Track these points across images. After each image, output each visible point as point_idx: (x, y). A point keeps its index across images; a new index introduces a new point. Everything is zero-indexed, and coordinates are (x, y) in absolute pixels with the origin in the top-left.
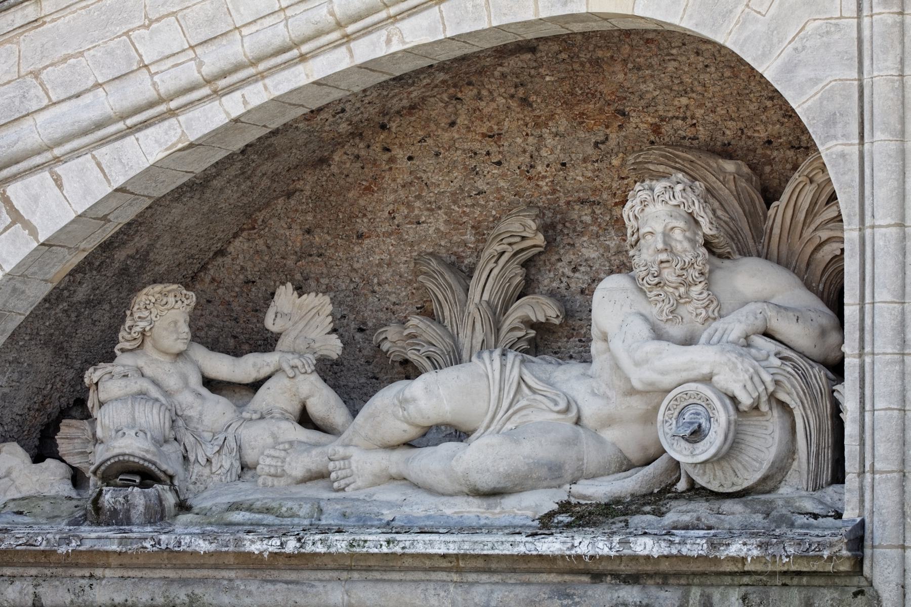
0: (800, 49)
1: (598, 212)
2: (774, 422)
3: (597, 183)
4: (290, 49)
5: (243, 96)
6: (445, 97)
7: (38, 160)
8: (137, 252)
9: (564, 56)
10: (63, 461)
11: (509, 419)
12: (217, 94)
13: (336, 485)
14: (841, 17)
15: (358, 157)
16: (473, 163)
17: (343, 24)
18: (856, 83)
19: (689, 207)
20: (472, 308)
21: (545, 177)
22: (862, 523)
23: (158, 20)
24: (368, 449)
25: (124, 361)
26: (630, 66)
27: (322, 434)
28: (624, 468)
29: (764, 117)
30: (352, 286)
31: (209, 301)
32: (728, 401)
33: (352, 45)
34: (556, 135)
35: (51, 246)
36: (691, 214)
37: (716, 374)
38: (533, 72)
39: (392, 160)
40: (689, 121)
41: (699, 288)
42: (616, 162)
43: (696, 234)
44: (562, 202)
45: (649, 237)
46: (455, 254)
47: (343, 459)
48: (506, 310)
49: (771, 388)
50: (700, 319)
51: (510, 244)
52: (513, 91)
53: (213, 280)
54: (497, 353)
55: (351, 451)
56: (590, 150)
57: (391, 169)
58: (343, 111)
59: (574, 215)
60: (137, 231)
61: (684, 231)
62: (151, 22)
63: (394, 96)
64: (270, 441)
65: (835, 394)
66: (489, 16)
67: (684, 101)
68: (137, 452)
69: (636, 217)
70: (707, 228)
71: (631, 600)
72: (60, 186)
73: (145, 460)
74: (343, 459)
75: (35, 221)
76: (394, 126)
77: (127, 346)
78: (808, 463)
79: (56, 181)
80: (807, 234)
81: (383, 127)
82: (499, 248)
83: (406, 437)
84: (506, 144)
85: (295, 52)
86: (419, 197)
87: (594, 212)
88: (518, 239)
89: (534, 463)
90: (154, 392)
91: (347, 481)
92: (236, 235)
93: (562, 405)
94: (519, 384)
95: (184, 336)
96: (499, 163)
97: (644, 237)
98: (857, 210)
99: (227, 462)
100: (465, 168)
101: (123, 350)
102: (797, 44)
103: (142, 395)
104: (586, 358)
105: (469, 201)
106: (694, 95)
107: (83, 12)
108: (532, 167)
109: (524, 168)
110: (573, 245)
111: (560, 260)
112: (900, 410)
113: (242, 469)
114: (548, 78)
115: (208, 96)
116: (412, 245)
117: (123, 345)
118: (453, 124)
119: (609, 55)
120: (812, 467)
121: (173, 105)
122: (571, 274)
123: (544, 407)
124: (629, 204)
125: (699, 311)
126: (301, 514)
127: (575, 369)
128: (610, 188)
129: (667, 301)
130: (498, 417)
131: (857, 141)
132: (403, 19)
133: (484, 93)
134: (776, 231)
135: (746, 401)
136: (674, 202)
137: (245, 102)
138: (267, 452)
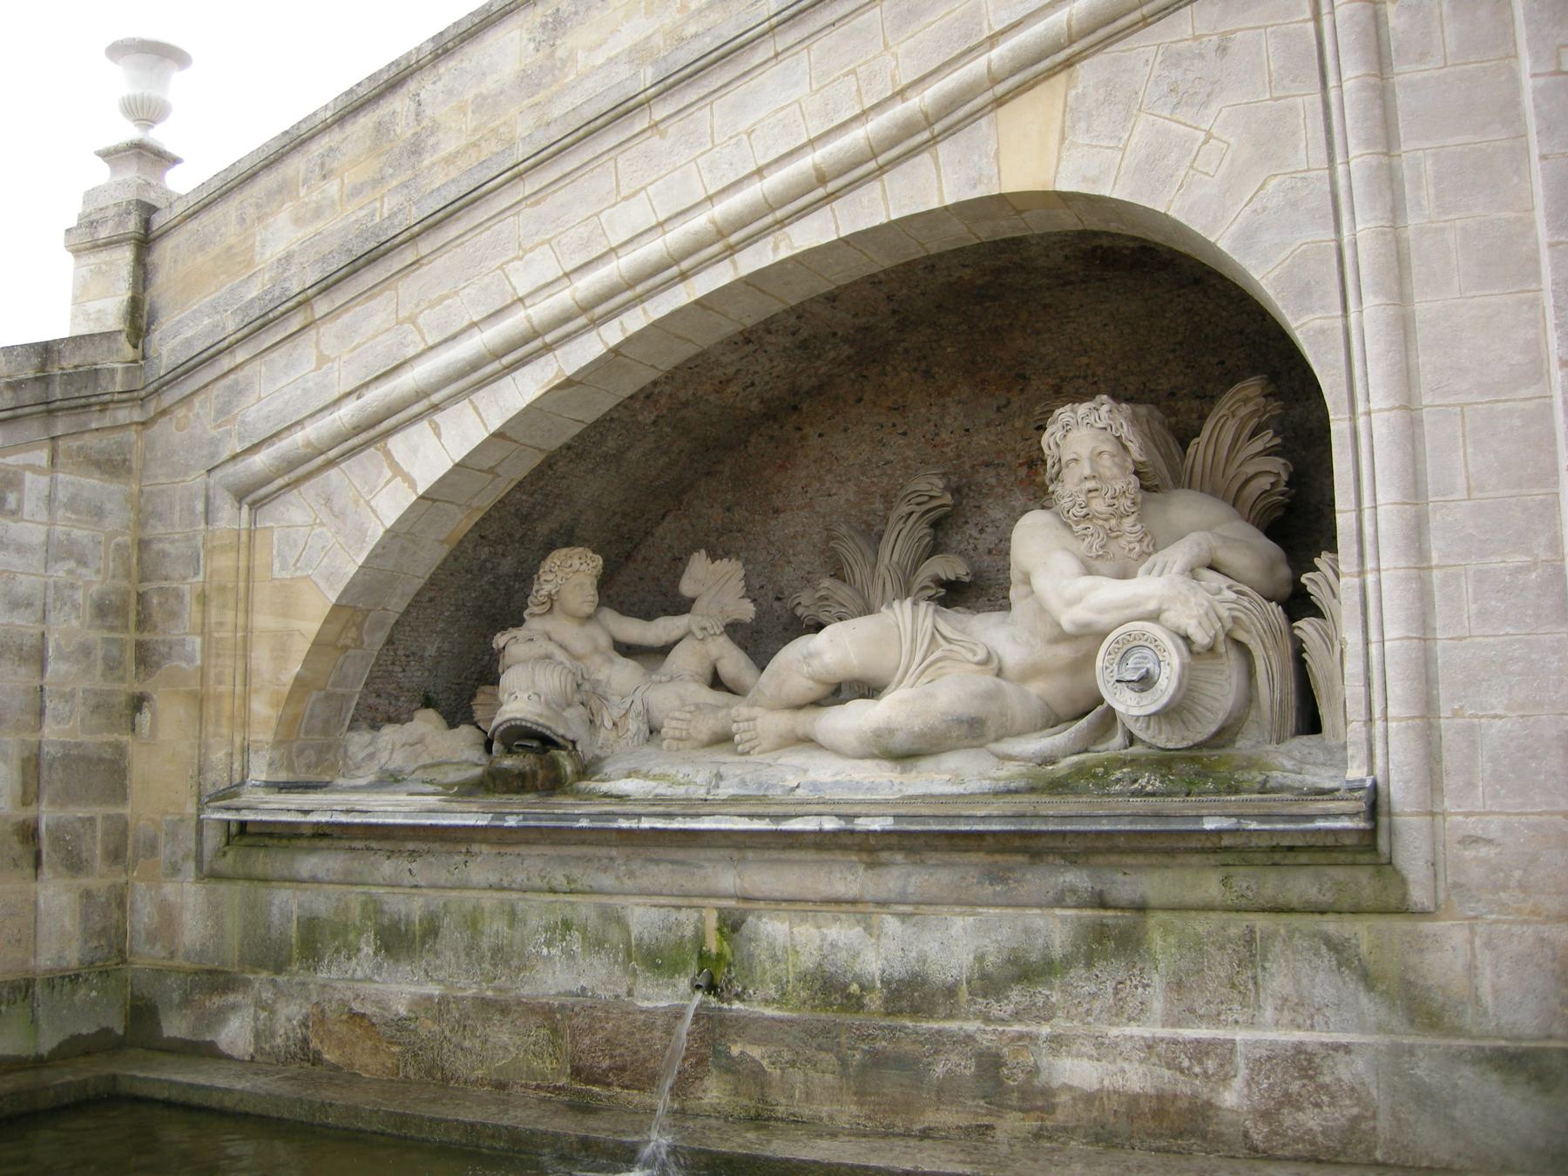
0: (1260, 210)
1: (1002, 473)
2: (1231, 666)
3: (1001, 445)
4: (669, 267)
5: (621, 323)
6: (852, 375)
7: (417, 408)
8: (561, 527)
9: (964, 327)
10: (479, 728)
11: (923, 672)
12: (595, 323)
13: (740, 748)
14: (1308, 170)
15: (772, 438)
16: (879, 435)
17: (725, 232)
18: (1333, 244)
19: (1117, 430)
20: (882, 569)
21: (949, 444)
22: (1375, 785)
23: (531, 250)
24: (773, 709)
25: (534, 625)
26: (1029, 331)
27: (730, 695)
28: (1051, 723)
29: (1166, 370)
30: (769, 558)
31: (641, 579)
32: (1180, 642)
33: (736, 256)
34: (959, 402)
35: (434, 501)
36: (1118, 438)
37: (1168, 610)
38: (934, 345)
39: (804, 438)
40: (1090, 379)
41: (1131, 520)
42: (1018, 424)
43: (1125, 461)
44: (967, 467)
45: (1073, 465)
46: (865, 522)
47: (747, 720)
48: (916, 569)
49: (1229, 625)
50: (1134, 555)
51: (919, 504)
52: (915, 364)
53: (645, 559)
54: (908, 602)
55: (757, 711)
56: (992, 415)
57: (802, 446)
58: (753, 384)
59: (979, 478)
60: (555, 503)
61: (1113, 456)
62: (526, 252)
63: (802, 372)
64: (677, 703)
65: (1297, 632)
66: (887, 209)
67: (1084, 360)
68: (529, 717)
69: (1057, 445)
70: (1136, 451)
71: (1080, 885)
72: (439, 436)
73: (538, 725)
74: (747, 720)
75: (415, 473)
76: (805, 406)
77: (537, 610)
78: (1272, 711)
79: (434, 429)
80: (1231, 471)
81: (795, 408)
82: (907, 509)
83: (812, 696)
84: (911, 415)
85: (675, 270)
86: (829, 471)
87: (998, 474)
88: (926, 498)
89: (953, 720)
90: (560, 656)
91: (752, 744)
92: (663, 517)
93: (981, 655)
94: (933, 634)
95: (590, 598)
96: (905, 434)
97: (1067, 466)
98: (1345, 396)
99: (634, 725)
100: (872, 441)
101: (533, 615)
102: (1256, 204)
103: (548, 657)
104: (1006, 606)
105: (877, 472)
106: (1094, 354)
107: (459, 250)
108: (936, 435)
109: (929, 436)
110: (979, 507)
111: (967, 522)
112: (1419, 639)
113: (651, 732)
114: (949, 350)
115: (585, 326)
116: (824, 517)
117: (533, 609)
118: (860, 400)
119: (1007, 322)
120: (1276, 718)
121: (549, 338)
122: (978, 536)
123: (960, 658)
124: (1049, 430)
125: (1131, 546)
126: (698, 780)
127: (994, 617)
128: (1014, 449)
129: (1096, 535)
130: (911, 671)
131: (1340, 313)
132: (791, 223)
133: (889, 368)
134: (1198, 469)
135: (1201, 638)
136: (1101, 425)
137: (623, 330)
138: (671, 715)
